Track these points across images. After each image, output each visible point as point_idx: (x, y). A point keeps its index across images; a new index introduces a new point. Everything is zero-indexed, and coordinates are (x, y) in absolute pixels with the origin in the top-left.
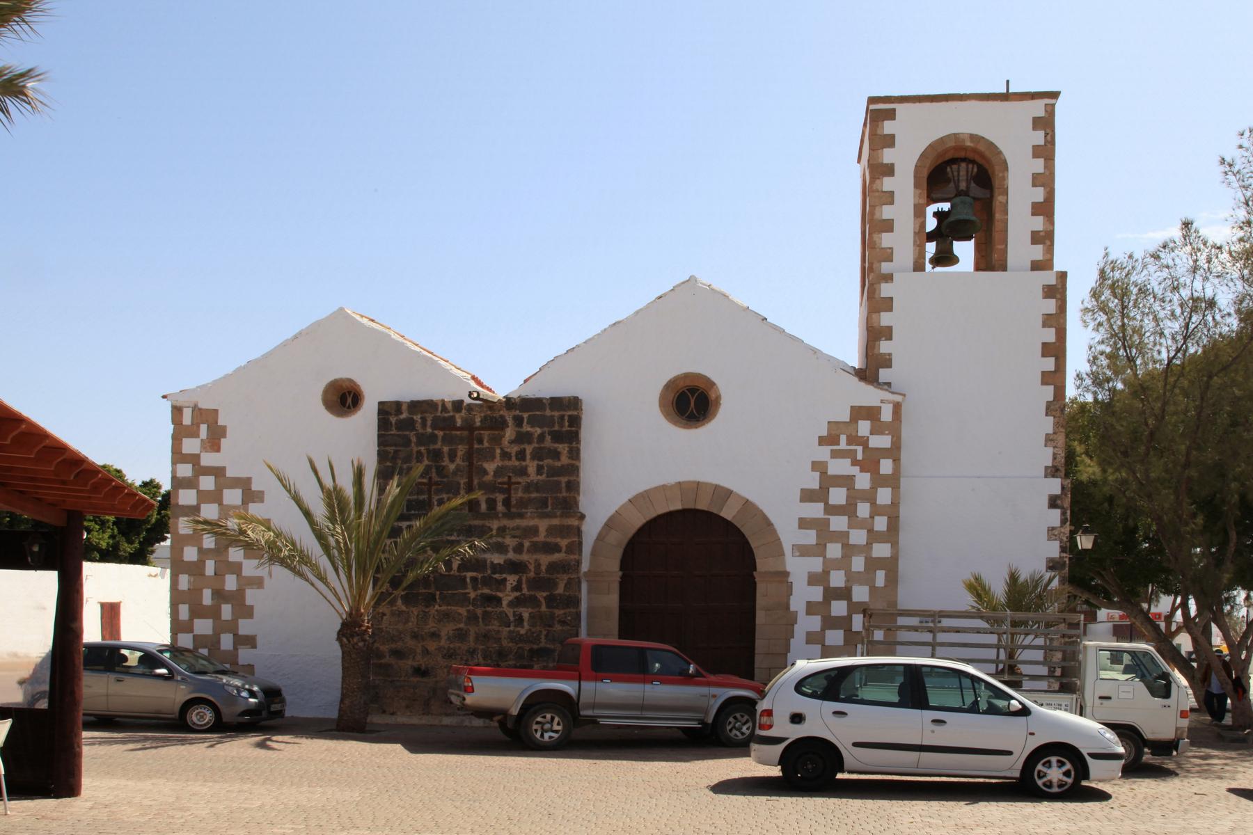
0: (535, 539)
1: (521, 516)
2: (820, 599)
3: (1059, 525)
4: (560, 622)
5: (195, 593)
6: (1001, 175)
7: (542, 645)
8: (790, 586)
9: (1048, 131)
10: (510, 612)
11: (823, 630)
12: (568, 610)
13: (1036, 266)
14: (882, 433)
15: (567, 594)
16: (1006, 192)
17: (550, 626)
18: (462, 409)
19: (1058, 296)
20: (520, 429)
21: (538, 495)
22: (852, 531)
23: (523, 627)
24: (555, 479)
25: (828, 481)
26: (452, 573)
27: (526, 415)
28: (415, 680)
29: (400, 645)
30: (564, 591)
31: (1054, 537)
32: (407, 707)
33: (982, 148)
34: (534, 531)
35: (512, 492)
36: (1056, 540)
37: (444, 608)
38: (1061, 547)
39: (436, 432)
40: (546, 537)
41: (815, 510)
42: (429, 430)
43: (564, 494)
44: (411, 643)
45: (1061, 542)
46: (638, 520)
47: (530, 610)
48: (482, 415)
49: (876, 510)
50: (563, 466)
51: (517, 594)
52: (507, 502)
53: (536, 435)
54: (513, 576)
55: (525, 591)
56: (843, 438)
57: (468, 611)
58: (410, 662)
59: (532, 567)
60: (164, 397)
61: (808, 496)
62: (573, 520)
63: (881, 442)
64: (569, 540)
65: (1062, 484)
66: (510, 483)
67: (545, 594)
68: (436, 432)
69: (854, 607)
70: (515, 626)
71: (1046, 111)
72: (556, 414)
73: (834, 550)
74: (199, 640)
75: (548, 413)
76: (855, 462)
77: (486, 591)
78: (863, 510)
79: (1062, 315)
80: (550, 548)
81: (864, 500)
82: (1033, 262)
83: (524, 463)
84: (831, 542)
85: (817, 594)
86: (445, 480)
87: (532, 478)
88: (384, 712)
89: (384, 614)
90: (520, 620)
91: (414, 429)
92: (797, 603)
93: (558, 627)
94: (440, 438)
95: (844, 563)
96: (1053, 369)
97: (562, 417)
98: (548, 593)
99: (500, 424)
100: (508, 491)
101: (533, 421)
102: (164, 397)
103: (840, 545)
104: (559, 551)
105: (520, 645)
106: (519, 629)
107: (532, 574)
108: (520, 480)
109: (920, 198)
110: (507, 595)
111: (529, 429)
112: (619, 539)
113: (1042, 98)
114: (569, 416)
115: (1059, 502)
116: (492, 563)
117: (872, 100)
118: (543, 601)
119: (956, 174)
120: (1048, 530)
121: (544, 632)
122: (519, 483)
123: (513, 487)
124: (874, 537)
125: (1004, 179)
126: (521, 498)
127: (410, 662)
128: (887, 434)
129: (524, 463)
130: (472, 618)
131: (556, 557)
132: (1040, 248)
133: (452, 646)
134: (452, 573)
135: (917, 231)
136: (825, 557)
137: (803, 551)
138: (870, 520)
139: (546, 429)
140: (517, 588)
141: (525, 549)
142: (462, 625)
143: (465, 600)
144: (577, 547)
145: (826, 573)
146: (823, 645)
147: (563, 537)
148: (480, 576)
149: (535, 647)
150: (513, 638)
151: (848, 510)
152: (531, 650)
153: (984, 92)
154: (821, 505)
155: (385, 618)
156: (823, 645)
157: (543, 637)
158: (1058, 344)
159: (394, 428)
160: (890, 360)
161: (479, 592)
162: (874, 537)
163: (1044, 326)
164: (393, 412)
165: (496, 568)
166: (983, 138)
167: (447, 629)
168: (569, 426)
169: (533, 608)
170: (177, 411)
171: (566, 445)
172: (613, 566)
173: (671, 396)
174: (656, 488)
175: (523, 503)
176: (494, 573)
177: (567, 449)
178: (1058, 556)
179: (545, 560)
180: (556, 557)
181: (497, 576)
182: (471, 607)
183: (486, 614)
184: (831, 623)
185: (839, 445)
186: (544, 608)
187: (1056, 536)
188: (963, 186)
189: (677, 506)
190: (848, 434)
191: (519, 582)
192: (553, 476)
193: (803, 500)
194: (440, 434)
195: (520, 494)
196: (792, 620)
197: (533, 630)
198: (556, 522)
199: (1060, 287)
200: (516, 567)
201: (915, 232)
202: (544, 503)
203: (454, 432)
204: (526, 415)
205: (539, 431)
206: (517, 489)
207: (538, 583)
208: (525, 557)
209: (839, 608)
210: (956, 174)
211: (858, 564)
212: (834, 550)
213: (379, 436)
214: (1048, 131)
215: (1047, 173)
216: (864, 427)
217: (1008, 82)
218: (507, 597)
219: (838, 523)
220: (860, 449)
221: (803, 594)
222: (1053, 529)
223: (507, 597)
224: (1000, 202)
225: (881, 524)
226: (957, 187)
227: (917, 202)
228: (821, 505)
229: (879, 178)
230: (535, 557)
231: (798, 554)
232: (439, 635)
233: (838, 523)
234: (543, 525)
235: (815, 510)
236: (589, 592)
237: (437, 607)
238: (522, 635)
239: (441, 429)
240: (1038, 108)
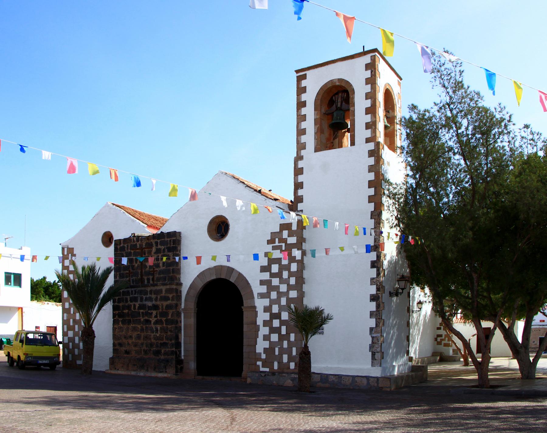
0: (161, 295)
1: (156, 285)
2: (268, 319)
3: (376, 277)
4: (170, 331)
5: (68, 320)
6: (352, 97)
7: (164, 341)
8: (256, 313)
9: (373, 69)
10: (153, 326)
11: (270, 334)
12: (172, 326)
13: (368, 140)
14: (293, 236)
15: (172, 318)
16: (354, 105)
17: (167, 333)
18: (139, 240)
19: (376, 155)
20: (157, 247)
21: (163, 276)
22: (280, 285)
23: (158, 333)
24: (169, 268)
25: (272, 261)
26: (136, 310)
27: (159, 241)
28: (125, 355)
29: (120, 341)
30: (171, 317)
31: (373, 283)
32: (122, 367)
33: (343, 85)
34: (161, 291)
35: (155, 275)
36: (374, 284)
37: (134, 325)
38: (377, 288)
39: (131, 251)
40: (165, 294)
41: (266, 276)
42: (129, 250)
43: (171, 275)
44: (124, 341)
45: (377, 286)
46: (200, 285)
47: (160, 326)
48: (145, 242)
49: (291, 274)
50: (171, 262)
51: (156, 319)
52: (153, 280)
53: (162, 249)
54: (155, 311)
55: (158, 318)
56: (277, 240)
57: (141, 327)
58: (124, 348)
59: (160, 307)
60: (60, 244)
61: (264, 269)
62: (173, 285)
63: (292, 240)
64: (172, 295)
65: (377, 255)
66: (154, 271)
67: (165, 319)
68: (131, 251)
69: (282, 323)
70: (156, 333)
71: (371, 59)
72: (169, 239)
73: (274, 295)
74: (69, 339)
75: (166, 239)
76: (282, 251)
77: (146, 318)
78: (285, 274)
79: (378, 165)
80: (166, 299)
81: (286, 270)
82: (366, 139)
83: (158, 262)
84: (273, 291)
85: (267, 316)
86: (134, 271)
87: (161, 268)
88: (115, 369)
89: (116, 328)
90: (157, 330)
91: (125, 250)
92: (260, 322)
93: (169, 333)
94: (132, 253)
95: (277, 301)
96: (374, 194)
97: (170, 240)
98: (166, 318)
99: (150, 246)
100: (153, 275)
101: (162, 243)
102: (60, 244)
103: (276, 292)
104: (169, 300)
105: (157, 341)
106: (157, 334)
107: (161, 310)
108: (157, 269)
109: (317, 115)
110: (153, 320)
111: (160, 247)
112: (195, 293)
113: (369, 53)
114: (173, 240)
115: (376, 264)
116: (148, 305)
117: (297, 71)
118: (164, 321)
119: (337, 99)
120: (371, 280)
121: (165, 336)
122: (157, 271)
123: (155, 272)
124: (290, 288)
125: (353, 98)
126: (158, 277)
127: (124, 348)
128: (295, 236)
129: (158, 262)
130: (142, 330)
131: (169, 302)
132: (369, 131)
133: (136, 341)
134: (136, 310)
135: (316, 132)
136: (270, 298)
137: (262, 296)
138: (288, 279)
139: (165, 246)
140: (156, 316)
141: (158, 300)
142: (139, 333)
143: (139, 322)
144: (179, 297)
145: (271, 306)
146: (270, 341)
147: (170, 294)
148: (144, 311)
149: (162, 342)
150: (156, 338)
151: (279, 275)
152: (161, 343)
153: (342, 57)
154: (268, 273)
155: (117, 330)
156: (270, 341)
157: (164, 338)
158: (376, 180)
159: (119, 251)
160: (302, 198)
161: (144, 318)
162: (290, 288)
163: (369, 172)
164: (119, 244)
165: (150, 308)
166: (344, 79)
167: (135, 334)
168: (173, 244)
169: (161, 325)
170: (63, 249)
171: (172, 253)
172: (192, 306)
173: (214, 227)
174: (207, 269)
175: (158, 279)
176: (149, 310)
177: (172, 254)
178: (375, 293)
179: (165, 303)
180: (169, 302)
181: (149, 311)
182: (142, 325)
183: (146, 327)
184: (273, 330)
185: (275, 243)
186: (164, 325)
187: (374, 282)
188: (339, 105)
189: (214, 277)
190: (279, 238)
191: (157, 313)
192: (168, 267)
193: (261, 271)
194: (132, 251)
195: (157, 276)
196: (257, 329)
197: (161, 334)
198: (168, 287)
199: (376, 150)
200: (155, 307)
201: (315, 133)
202: (165, 279)
203: (137, 251)
204: (159, 241)
205: (163, 247)
206: (156, 273)
207: (164, 314)
208: (158, 303)
209: (276, 323)
210: (337, 99)
211: (283, 301)
212: (274, 295)
213: (115, 254)
214: (373, 69)
215: (373, 92)
216: (285, 233)
217: (364, 47)
218: (153, 320)
219: (275, 282)
220: (283, 245)
221: (262, 317)
222: (373, 279)
223: (153, 320)
224: (352, 111)
225: (293, 281)
226: (336, 106)
227: (316, 118)
228: (268, 273)
229: (300, 109)
230: (162, 302)
231: (260, 297)
232: (132, 337)
233: (275, 282)
234: (164, 288)
235: (266, 276)
236: (184, 318)
237: (132, 325)
238: (157, 337)
239: (133, 250)
240: (367, 59)
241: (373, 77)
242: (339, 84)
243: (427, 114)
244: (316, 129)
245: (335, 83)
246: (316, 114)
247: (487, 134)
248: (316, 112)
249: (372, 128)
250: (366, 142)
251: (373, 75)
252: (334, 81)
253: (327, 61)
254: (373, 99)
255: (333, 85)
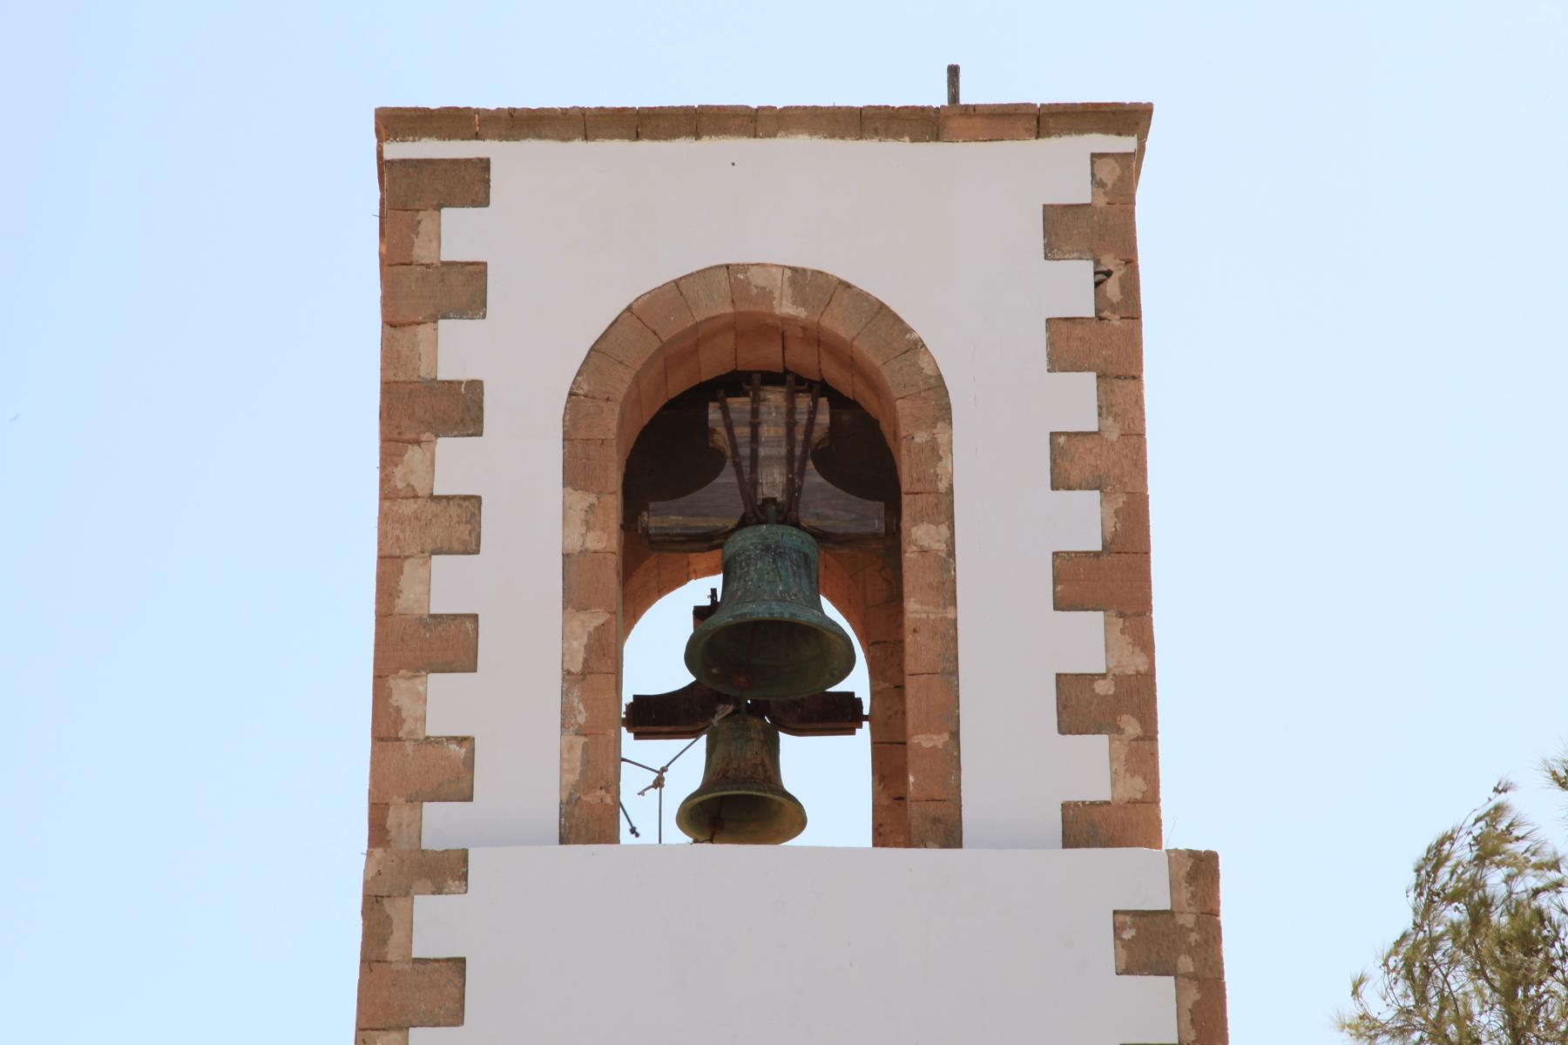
6: (921, 437)
9: (1109, 262)
19: (1186, 964)
33: (839, 324)
109: (588, 526)
117: (392, 123)
119: (743, 432)
125: (936, 452)
132: (1096, 747)
135: (577, 667)
188: (772, 482)
199: (1188, 920)
210: (743, 432)
215: (1114, 434)
224: (923, 551)
226: (749, 487)
227: (576, 545)
241: (1116, 321)
242: (801, 313)
243: (421, 562)
244: (579, 645)
245: (766, 294)
246: (578, 516)
247: (1512, 915)
248: (582, 500)
249: (1119, 730)
250: (1071, 839)
251: (1114, 308)
252: (758, 279)
253: (695, 101)
254: (1121, 500)
255: (745, 307)
